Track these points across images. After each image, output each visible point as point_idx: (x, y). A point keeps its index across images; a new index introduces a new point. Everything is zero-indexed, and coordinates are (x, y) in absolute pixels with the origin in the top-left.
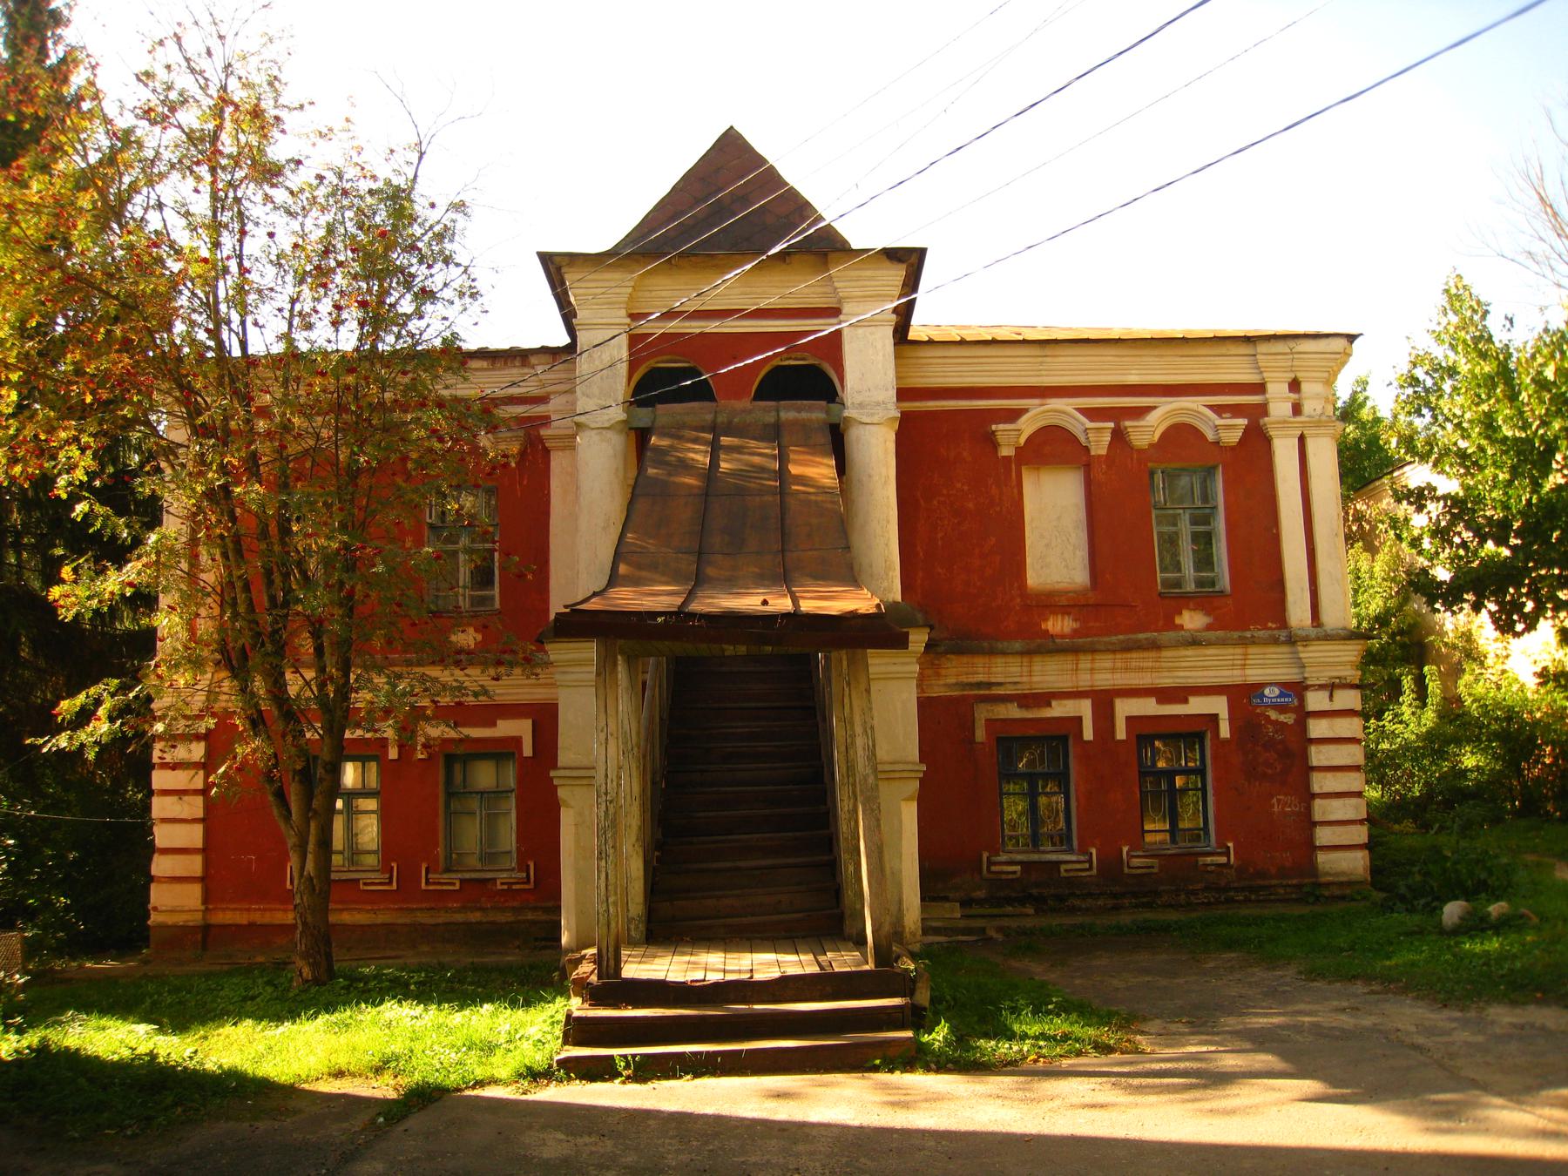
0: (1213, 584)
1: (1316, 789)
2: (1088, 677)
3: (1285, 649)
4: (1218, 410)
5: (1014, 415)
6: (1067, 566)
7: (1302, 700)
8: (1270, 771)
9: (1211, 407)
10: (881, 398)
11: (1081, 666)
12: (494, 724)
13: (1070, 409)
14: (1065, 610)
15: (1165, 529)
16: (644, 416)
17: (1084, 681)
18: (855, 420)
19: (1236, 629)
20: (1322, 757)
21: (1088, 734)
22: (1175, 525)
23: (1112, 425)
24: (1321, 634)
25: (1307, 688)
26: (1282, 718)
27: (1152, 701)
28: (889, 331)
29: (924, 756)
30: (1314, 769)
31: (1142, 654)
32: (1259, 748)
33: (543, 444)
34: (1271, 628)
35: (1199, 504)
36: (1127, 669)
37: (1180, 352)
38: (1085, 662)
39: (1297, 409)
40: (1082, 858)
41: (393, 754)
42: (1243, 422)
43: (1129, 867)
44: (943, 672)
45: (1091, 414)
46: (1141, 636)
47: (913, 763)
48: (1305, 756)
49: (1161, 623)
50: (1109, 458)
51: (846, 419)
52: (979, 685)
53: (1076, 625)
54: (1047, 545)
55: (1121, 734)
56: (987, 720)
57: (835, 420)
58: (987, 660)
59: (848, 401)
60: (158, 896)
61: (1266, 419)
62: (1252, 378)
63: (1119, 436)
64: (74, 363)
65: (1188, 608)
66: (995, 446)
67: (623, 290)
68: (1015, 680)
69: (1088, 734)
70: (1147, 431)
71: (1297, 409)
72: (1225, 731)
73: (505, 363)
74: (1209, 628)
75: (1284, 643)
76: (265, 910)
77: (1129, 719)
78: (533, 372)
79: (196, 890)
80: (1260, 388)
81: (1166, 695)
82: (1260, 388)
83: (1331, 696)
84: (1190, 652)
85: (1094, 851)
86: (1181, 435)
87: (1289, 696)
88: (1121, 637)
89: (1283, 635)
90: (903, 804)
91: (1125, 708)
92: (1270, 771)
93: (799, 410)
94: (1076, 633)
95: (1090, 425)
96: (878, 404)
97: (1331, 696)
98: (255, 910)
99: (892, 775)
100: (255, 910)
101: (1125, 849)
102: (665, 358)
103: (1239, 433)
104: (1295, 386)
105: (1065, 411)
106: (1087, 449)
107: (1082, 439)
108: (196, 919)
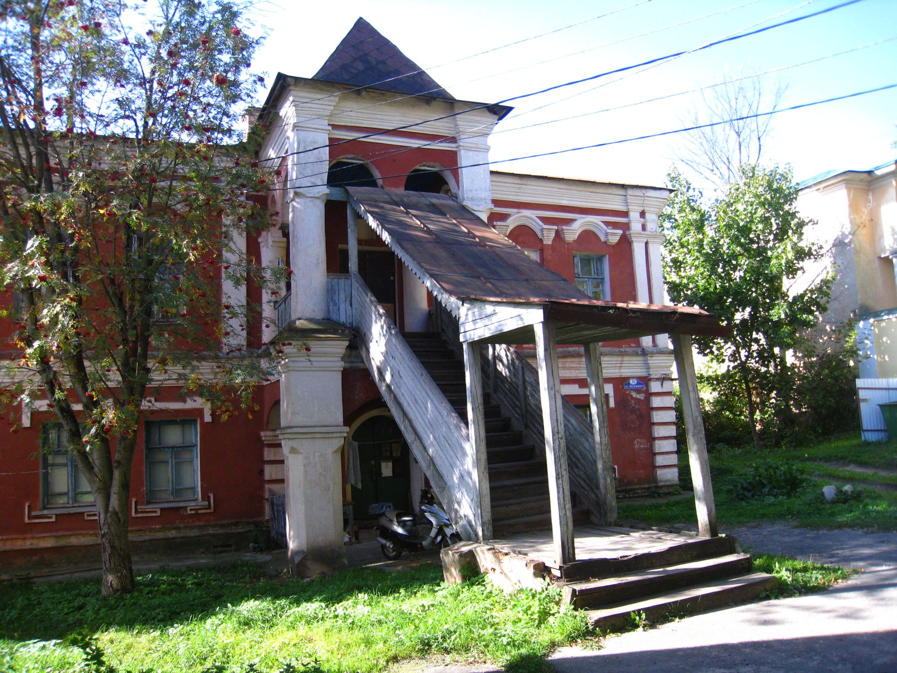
3: (641, 358)
7: (647, 386)
13: (534, 217)
23: (556, 227)
25: (650, 380)
26: (638, 396)
30: (654, 424)
42: (620, 232)
45: (545, 220)
48: (649, 417)
50: (553, 247)
62: (623, 208)
67: (328, 107)
70: (572, 233)
80: (625, 214)
82: (625, 214)
83: (662, 384)
86: (588, 236)
96: (482, 199)
97: (662, 384)
103: (618, 238)
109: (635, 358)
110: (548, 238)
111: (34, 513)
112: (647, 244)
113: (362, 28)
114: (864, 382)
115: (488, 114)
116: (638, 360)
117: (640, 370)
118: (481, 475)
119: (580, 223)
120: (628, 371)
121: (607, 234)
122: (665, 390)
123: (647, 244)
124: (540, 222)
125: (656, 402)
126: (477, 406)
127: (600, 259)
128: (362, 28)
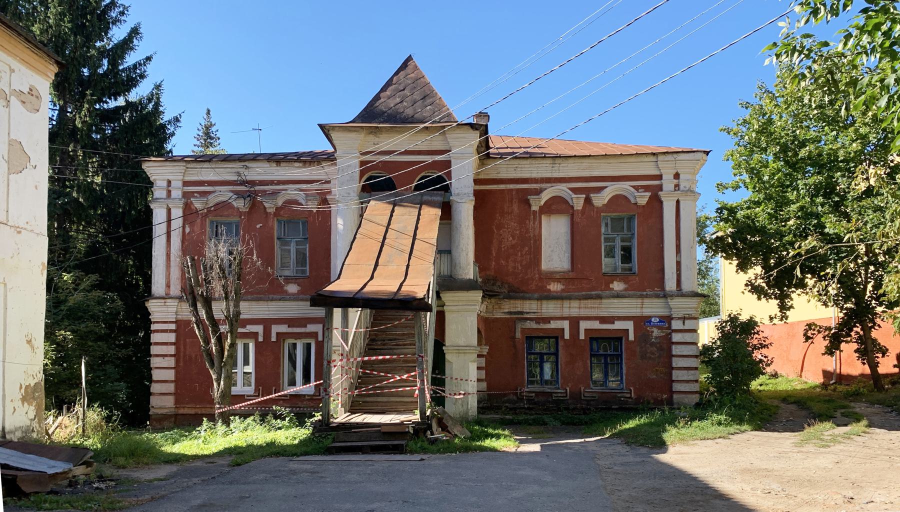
1: (674, 365)
2: (568, 310)
3: (662, 300)
4: (636, 188)
5: (538, 192)
6: (561, 261)
8: (653, 356)
9: (633, 187)
10: (466, 192)
11: (564, 306)
12: (306, 326)
13: (565, 188)
14: (558, 280)
17: (566, 312)
20: (677, 351)
21: (567, 336)
23: (584, 196)
24: (680, 293)
25: (672, 319)
27: (598, 322)
30: (673, 356)
31: (593, 301)
37: (619, 161)
38: (566, 303)
39: (677, 186)
41: (261, 339)
42: (648, 194)
43: (584, 396)
44: (503, 307)
45: (575, 190)
46: (593, 293)
47: (475, 347)
48: (670, 350)
50: (583, 211)
53: (563, 287)
54: (552, 251)
55: (582, 336)
58: (522, 302)
60: (154, 401)
62: (655, 172)
63: (588, 201)
65: (616, 281)
66: (530, 206)
67: (356, 142)
69: (567, 336)
70: (600, 200)
71: (677, 186)
72: (631, 337)
73: (310, 165)
74: (626, 290)
75: (662, 297)
76: (202, 408)
77: (278, 334)
80: (660, 177)
81: (603, 320)
82: (660, 177)
83: (684, 323)
84: (616, 300)
85: (568, 389)
86: (618, 200)
87: (664, 322)
88: (584, 293)
90: (470, 364)
91: (584, 325)
92: (653, 356)
95: (574, 196)
96: (465, 194)
97: (684, 323)
98: (198, 408)
99: (466, 351)
100: (198, 408)
102: (376, 171)
103: (647, 199)
104: (677, 176)
105: (561, 190)
106: (572, 207)
108: (172, 411)
109: (656, 300)
114: (686, 338)
115: (471, 131)
116: (658, 302)
117: (662, 310)
119: (611, 190)
120: (650, 310)
121: (635, 197)
122: (686, 327)
123: (678, 202)
124: (570, 192)
127: (630, 219)
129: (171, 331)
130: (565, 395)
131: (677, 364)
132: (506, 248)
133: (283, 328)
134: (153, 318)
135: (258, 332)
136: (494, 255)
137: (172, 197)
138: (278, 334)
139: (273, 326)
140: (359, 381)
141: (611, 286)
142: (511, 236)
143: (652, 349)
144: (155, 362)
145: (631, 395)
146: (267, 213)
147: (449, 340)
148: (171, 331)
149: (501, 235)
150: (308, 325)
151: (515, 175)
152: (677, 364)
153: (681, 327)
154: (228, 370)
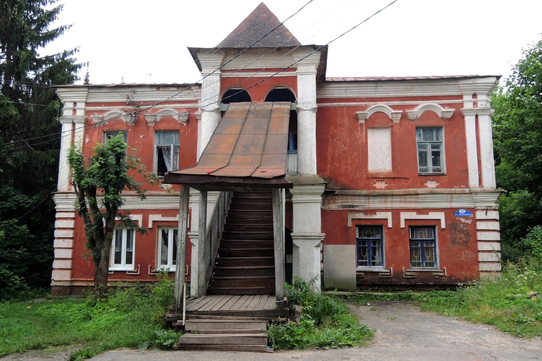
0: (440, 171)
7: (474, 215)
9: (441, 105)
10: (310, 101)
13: (386, 106)
15: (421, 150)
16: (225, 107)
17: (389, 205)
18: (301, 109)
19: (448, 188)
20: (482, 237)
21: (390, 225)
22: (426, 148)
23: (401, 111)
25: (477, 210)
26: (466, 221)
27: (415, 213)
28: (314, 77)
29: (323, 229)
32: (457, 233)
33: (195, 117)
34: (462, 188)
35: (435, 141)
36: (405, 202)
40: (387, 271)
42: (453, 110)
44: (337, 201)
45: (394, 107)
46: (411, 190)
48: (475, 236)
49: (419, 185)
51: (298, 108)
52: (350, 206)
54: (376, 156)
55: (403, 225)
56: (352, 219)
57: (293, 109)
59: (299, 102)
61: (463, 109)
64: (535, 102)
67: (218, 61)
68: (363, 204)
69: (390, 225)
72: (443, 226)
74: (438, 187)
77: (154, 222)
78: (192, 92)
79: (68, 273)
81: (419, 211)
83: (486, 213)
85: (392, 269)
87: (469, 213)
88: (403, 190)
89: (467, 190)
91: (404, 216)
93: (280, 105)
94: (386, 188)
95: (393, 111)
97: (486, 213)
101: (404, 268)
106: (392, 120)
107: (390, 117)
110: (397, 119)
111: (152, 271)
112: (477, 116)
113: (262, 9)
118: (200, 261)
125: (480, 226)
126: (201, 224)
128: (262, 9)
129: (71, 219)
130: (389, 274)
131: (482, 248)
132: (339, 153)
133: (158, 217)
134: (58, 207)
135: (138, 221)
136: (329, 159)
137: (77, 115)
138: (154, 222)
139: (391, 213)
140: (217, 263)
141: (426, 184)
142: (343, 143)
143: (460, 235)
144: (57, 243)
145: (444, 274)
146: (148, 127)
147: (297, 230)
148: (71, 219)
149: (335, 143)
150: (430, 213)
151: (345, 95)
152: (482, 248)
153: (484, 217)
154: (106, 251)
